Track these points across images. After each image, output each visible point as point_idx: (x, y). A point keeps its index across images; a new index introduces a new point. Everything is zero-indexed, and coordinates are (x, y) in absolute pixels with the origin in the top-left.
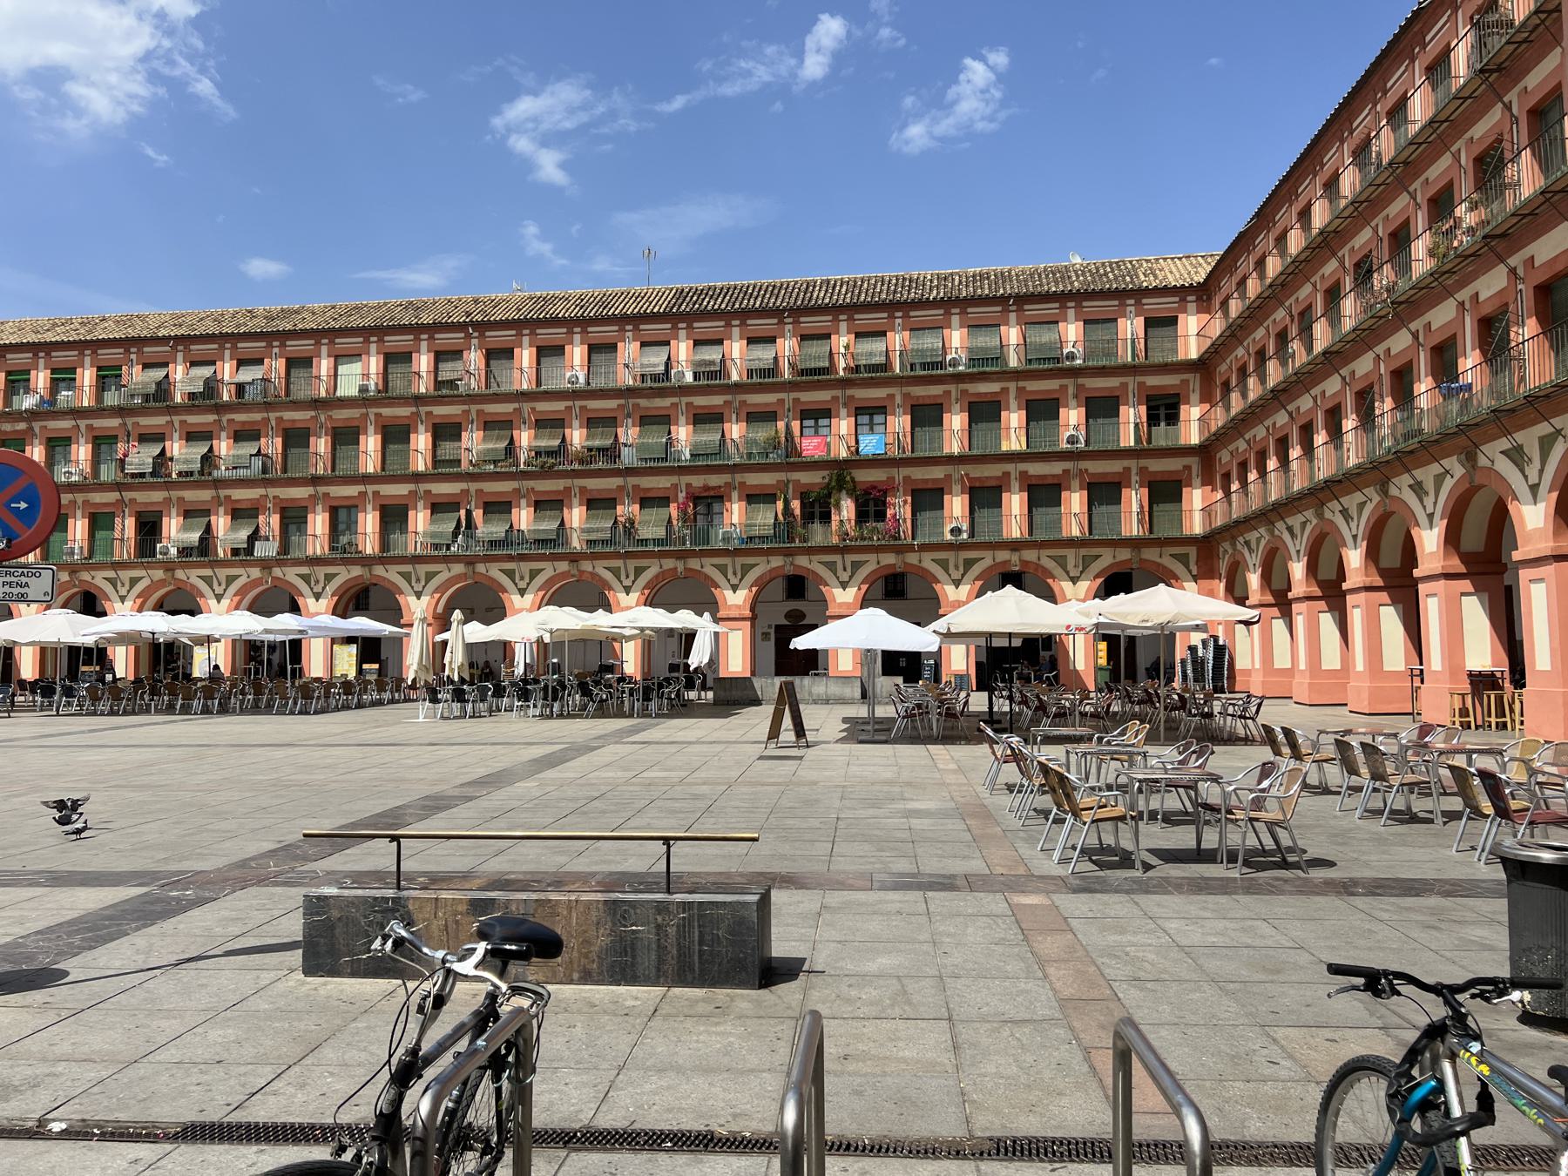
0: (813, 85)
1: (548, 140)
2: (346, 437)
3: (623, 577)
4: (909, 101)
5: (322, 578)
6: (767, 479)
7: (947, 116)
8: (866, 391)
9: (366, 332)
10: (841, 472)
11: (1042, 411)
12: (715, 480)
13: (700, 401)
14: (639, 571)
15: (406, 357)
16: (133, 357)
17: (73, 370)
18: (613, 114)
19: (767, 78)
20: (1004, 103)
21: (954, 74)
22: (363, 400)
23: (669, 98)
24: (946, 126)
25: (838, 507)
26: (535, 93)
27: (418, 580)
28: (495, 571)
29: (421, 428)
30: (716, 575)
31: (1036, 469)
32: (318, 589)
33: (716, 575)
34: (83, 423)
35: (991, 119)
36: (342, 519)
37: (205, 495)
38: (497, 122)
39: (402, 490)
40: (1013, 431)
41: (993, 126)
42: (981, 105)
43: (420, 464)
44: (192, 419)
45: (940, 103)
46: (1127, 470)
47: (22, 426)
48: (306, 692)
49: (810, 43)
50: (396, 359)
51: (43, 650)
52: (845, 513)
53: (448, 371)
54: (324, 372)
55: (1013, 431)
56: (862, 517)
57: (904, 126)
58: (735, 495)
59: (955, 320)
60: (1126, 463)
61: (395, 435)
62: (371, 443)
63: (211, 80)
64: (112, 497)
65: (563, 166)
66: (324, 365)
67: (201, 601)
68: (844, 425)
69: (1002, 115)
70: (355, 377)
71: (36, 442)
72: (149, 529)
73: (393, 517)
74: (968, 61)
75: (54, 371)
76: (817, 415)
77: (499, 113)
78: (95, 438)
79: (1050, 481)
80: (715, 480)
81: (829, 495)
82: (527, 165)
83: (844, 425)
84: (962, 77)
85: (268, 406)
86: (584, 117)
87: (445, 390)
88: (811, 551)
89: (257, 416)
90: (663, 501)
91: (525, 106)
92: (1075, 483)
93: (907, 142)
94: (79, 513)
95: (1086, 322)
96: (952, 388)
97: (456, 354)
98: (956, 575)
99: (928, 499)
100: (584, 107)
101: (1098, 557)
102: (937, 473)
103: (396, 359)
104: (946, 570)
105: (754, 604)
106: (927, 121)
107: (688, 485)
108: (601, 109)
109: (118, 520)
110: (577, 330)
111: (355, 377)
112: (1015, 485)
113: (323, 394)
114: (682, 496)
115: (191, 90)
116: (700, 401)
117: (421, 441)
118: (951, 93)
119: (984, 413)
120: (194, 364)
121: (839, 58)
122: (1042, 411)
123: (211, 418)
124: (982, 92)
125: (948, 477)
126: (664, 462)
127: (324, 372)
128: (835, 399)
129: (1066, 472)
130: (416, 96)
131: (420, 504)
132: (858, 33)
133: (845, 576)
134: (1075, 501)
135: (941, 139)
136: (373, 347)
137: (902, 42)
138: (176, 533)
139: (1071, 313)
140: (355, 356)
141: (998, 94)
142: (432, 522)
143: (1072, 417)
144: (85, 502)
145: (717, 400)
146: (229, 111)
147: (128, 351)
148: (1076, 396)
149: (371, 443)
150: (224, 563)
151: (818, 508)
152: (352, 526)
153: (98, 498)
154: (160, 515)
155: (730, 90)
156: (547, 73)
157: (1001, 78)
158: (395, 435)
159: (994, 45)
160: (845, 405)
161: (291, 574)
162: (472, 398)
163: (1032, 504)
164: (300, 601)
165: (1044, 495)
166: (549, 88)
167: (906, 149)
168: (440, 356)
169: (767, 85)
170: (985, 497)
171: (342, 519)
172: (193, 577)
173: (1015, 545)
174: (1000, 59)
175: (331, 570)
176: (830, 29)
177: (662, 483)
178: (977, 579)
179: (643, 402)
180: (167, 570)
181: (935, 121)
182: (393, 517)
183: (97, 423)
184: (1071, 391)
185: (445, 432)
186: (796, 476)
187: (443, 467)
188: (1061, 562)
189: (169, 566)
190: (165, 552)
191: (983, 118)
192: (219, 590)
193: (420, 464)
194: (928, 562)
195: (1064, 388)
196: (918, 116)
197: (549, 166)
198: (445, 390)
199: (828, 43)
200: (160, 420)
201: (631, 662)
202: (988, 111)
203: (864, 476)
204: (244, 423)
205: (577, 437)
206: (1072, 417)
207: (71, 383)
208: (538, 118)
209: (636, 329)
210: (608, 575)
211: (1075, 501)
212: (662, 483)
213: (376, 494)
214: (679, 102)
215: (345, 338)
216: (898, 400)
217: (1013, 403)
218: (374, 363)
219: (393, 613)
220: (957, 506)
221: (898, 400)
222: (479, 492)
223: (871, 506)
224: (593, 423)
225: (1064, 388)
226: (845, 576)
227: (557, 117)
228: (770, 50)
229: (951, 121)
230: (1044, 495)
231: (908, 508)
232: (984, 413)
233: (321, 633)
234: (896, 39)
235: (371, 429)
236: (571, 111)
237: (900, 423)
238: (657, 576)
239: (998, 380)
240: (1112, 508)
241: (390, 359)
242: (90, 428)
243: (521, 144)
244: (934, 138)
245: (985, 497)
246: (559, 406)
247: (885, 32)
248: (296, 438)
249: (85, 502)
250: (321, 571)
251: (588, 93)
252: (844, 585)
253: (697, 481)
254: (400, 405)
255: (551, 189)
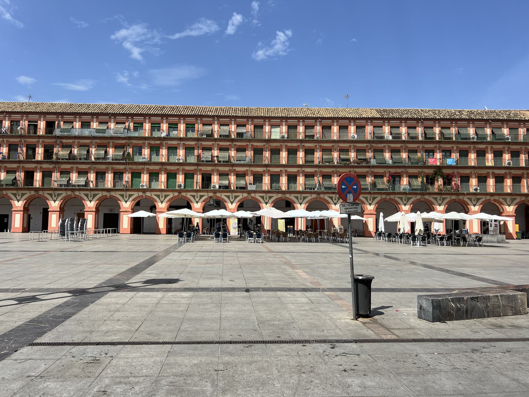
0: (230, 36)
1: (136, 44)
2: (276, 152)
3: (369, 200)
4: (260, 44)
5: (268, 197)
6: (415, 171)
7: (270, 49)
8: (446, 146)
9: (282, 118)
10: (438, 170)
11: (498, 154)
12: (399, 170)
13: (393, 145)
14: (374, 199)
15: (295, 127)
16: (199, 121)
17: (177, 124)
18: (153, 38)
19: (207, 31)
20: (289, 47)
21: (275, 36)
22: (282, 140)
23: (173, 34)
24: (270, 52)
25: (438, 181)
26: (127, 29)
27: (55, 196)
28: (326, 197)
29: (301, 150)
30: (399, 201)
31: (497, 172)
32: (266, 201)
33: (399, 201)
34: (147, 142)
35: (285, 51)
36: (275, 178)
37: (226, 169)
38: (113, 37)
39: (295, 170)
40: (490, 160)
41: (285, 54)
42: (282, 47)
43: (284, 162)
44: (221, 143)
45: (269, 45)
46: (523, 173)
47: (158, 142)
48: (329, 234)
49: (230, 22)
50: (292, 128)
51: (202, 219)
52: (440, 182)
53: (309, 132)
54: (267, 131)
55: (490, 160)
56: (445, 184)
57: (256, 52)
58: (405, 175)
59: (471, 125)
60: (523, 171)
61: (292, 152)
62: (284, 154)
63: (10, 14)
64: (193, 168)
65: (141, 54)
66: (267, 128)
67: (261, 205)
68: (438, 155)
69: (288, 51)
70: (278, 133)
71: (5, 146)
72: (207, 180)
73: (292, 178)
74: (278, 32)
75: (169, 124)
76: (430, 152)
77: (113, 34)
78: (168, 147)
79: (501, 175)
80: (399, 170)
81: (434, 177)
82: (129, 52)
83: (438, 155)
84: (277, 37)
85: (249, 141)
86: (143, 38)
87: (310, 138)
88: (430, 194)
89: (244, 144)
90: (382, 176)
91: (123, 33)
92: (508, 177)
93: (257, 56)
94: (181, 173)
95: (510, 129)
96: (386, 145)
97: (312, 127)
98: (474, 203)
99: (465, 179)
100: (144, 34)
101: (516, 199)
102: (467, 171)
103: (292, 128)
104: (471, 201)
105: (516, 211)
106: (264, 50)
107: (390, 172)
108: (149, 36)
109: (195, 176)
110: (335, 121)
111: (278, 133)
112: (491, 176)
113: (267, 138)
114: (387, 175)
115: (3, 17)
116: (393, 145)
117: (301, 154)
118: (273, 42)
119: (481, 154)
120: (117, 123)
121: (240, 28)
122: (498, 154)
123: (228, 143)
124: (283, 43)
125: (471, 173)
126: (382, 165)
127: (267, 131)
128: (436, 147)
129: (506, 173)
130: (85, 25)
131: (301, 175)
132: (246, 20)
133: (440, 202)
134: (509, 182)
135: (267, 56)
136: (284, 123)
137: (260, 25)
138: (215, 180)
139: (505, 125)
140: (278, 126)
141: (288, 44)
142: (237, 180)
143: (507, 157)
144: (183, 169)
145: (398, 145)
146: (20, 25)
147: (197, 119)
148: (508, 150)
149: (284, 154)
150: (233, 191)
151: (431, 181)
152: (278, 181)
153: (187, 168)
154: (211, 174)
155: (194, 33)
156: (131, 22)
157: (289, 39)
158: (292, 152)
159: (287, 29)
160: (439, 149)
161: (189, 195)
162: (317, 141)
163: (496, 182)
164: (191, 204)
165: (499, 180)
166: (133, 27)
167: (256, 58)
168: (307, 127)
169: (207, 33)
170: (482, 180)
171: (275, 178)
172: (223, 196)
173: (108, 190)
174: (289, 33)
175: (271, 195)
176: (237, 18)
177: (381, 170)
178: (481, 204)
179: (374, 145)
180: (35, 191)
181: (267, 50)
182: (292, 178)
183: (187, 143)
184: (506, 149)
185: (309, 152)
186: (424, 170)
187: (309, 163)
188: (505, 200)
189: (215, 192)
190: (214, 187)
191: (282, 51)
192: (232, 200)
193: (284, 162)
194: (466, 199)
195: (504, 148)
196: (262, 48)
197: (136, 53)
198: (310, 138)
199: (236, 22)
200: (210, 143)
201: (267, 226)
202: (284, 49)
203: (446, 171)
204: (240, 146)
205: (352, 155)
206: (507, 157)
207: (159, 129)
208: (130, 36)
209: (371, 122)
210: (155, 197)
211: (509, 182)
212: (381, 170)
213: (286, 171)
214: (177, 36)
215: (275, 121)
216: (455, 148)
217: (489, 152)
218: (284, 128)
219: (153, 208)
220: (474, 182)
221: (455, 148)
222: (321, 171)
223: (448, 180)
224: (358, 151)
225: (504, 148)
226: (440, 202)
227: (134, 37)
228: (209, 22)
229: (272, 51)
230: (499, 180)
231: (459, 182)
232: (481, 154)
233: (232, 214)
234: (258, 24)
235: (284, 150)
236: (139, 35)
237: (455, 156)
238: (380, 200)
239: (485, 144)
240: (519, 184)
241: (290, 127)
242: (149, 143)
243: (127, 45)
244: (265, 55)
245: (482, 180)
246: (347, 145)
247: (255, 21)
248: (258, 152)
249: (183, 169)
250: (164, 194)
251: (146, 30)
252: (370, 204)
253: (393, 171)
254: (294, 143)
255: (136, 61)
